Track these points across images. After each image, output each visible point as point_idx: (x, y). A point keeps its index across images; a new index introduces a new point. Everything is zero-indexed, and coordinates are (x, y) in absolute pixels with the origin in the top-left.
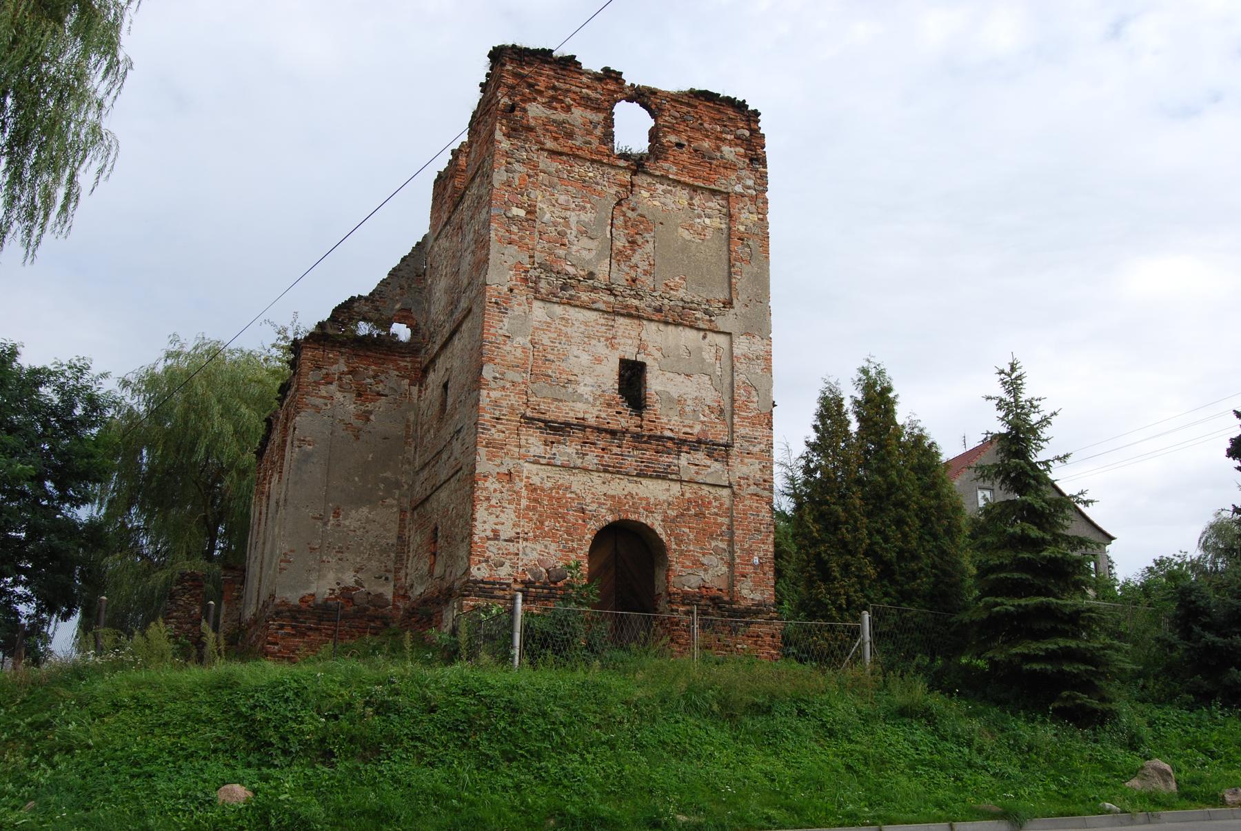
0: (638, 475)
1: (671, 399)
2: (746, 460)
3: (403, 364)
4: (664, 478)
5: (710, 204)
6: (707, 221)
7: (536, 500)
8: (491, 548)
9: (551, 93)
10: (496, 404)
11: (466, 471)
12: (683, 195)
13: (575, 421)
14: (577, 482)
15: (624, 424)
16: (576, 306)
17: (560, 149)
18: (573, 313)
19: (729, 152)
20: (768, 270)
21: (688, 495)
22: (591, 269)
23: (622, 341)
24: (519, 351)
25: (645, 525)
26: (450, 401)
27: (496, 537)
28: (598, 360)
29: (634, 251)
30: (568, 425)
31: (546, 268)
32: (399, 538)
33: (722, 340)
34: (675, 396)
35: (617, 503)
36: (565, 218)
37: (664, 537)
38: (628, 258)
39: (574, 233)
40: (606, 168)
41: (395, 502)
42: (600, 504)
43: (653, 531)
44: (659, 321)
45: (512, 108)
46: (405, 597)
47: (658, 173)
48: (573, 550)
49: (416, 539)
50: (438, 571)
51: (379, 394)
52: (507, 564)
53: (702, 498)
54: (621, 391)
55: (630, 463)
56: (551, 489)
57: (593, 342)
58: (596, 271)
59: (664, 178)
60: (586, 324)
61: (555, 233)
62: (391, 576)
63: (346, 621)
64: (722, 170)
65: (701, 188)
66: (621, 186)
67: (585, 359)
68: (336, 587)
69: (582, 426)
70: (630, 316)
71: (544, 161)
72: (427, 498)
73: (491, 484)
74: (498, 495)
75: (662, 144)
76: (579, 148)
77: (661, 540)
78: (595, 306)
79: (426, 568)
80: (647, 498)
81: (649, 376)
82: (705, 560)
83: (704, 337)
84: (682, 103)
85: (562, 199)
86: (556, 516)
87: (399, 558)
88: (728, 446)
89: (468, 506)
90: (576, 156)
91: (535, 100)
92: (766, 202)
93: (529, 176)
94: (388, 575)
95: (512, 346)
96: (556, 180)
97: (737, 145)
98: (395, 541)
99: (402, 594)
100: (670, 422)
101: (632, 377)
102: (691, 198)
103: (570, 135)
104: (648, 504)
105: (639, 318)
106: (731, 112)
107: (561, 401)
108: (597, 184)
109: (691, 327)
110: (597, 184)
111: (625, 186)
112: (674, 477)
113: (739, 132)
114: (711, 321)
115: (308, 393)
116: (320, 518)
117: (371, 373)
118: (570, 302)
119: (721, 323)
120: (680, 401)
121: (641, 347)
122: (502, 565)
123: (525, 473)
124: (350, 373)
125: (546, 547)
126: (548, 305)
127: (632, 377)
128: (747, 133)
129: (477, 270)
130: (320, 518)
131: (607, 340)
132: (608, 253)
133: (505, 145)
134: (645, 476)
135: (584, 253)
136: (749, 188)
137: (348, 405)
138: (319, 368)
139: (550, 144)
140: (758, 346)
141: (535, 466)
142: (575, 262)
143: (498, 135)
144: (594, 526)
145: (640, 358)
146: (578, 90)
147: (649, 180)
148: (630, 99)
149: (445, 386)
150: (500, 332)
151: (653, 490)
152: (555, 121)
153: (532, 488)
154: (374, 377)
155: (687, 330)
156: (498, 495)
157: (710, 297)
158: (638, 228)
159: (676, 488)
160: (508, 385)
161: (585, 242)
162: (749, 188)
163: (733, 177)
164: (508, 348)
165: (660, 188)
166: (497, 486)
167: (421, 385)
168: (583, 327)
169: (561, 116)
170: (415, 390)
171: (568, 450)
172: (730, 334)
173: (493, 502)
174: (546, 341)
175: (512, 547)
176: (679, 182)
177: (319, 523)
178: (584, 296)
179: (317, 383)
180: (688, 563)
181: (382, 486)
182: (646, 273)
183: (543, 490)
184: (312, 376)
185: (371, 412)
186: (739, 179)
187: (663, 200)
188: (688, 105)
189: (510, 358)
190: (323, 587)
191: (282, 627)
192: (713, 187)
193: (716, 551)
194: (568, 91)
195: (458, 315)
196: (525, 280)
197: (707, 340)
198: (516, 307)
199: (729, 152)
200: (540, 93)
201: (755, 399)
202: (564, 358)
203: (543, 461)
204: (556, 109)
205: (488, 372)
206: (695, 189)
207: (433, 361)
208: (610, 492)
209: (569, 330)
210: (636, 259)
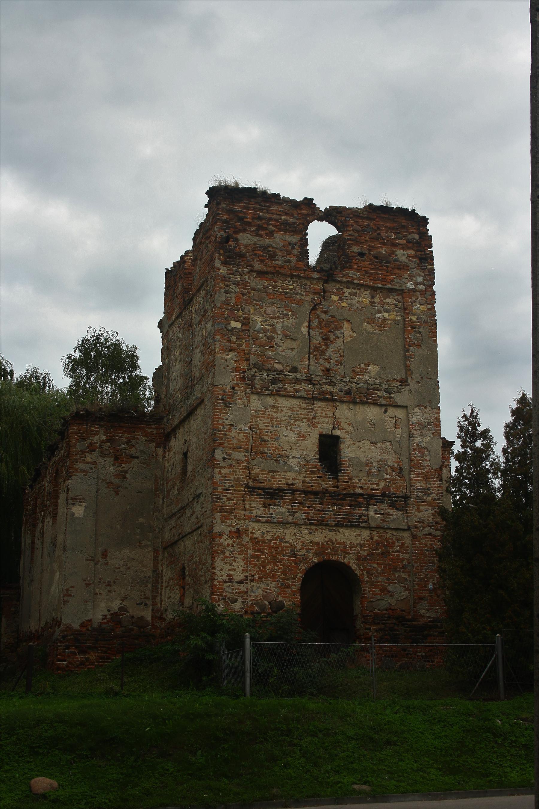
0: (336, 525)
1: (360, 464)
2: (421, 508)
3: (149, 431)
4: (357, 526)
5: (388, 300)
6: (386, 315)
7: (259, 550)
8: (227, 589)
9: (257, 222)
10: (225, 478)
11: (205, 529)
12: (366, 294)
13: (286, 487)
14: (290, 535)
15: (324, 486)
16: (284, 396)
17: (266, 269)
18: (284, 403)
19: (401, 255)
20: (436, 351)
21: (376, 538)
22: (294, 365)
23: (321, 420)
24: (241, 435)
25: (344, 564)
26: (190, 468)
27: (230, 579)
28: (302, 437)
29: (327, 346)
30: (281, 490)
31: (259, 367)
32: (154, 571)
33: (400, 413)
34: (364, 460)
35: (320, 548)
36: (272, 325)
37: (358, 572)
38: (323, 352)
39: (280, 337)
40: (304, 281)
41: (149, 543)
42: (308, 550)
43: (350, 568)
44: (349, 402)
45: (227, 239)
46: (161, 618)
47: (344, 280)
48: (289, 586)
49: (167, 574)
50: (187, 601)
51: (132, 457)
52: (240, 600)
53: (387, 540)
54: (321, 460)
55: (330, 516)
56: (270, 541)
57: (298, 423)
58: (299, 366)
59: (349, 284)
60: (291, 409)
61: (265, 338)
62: (149, 602)
63: (124, 645)
64: (397, 271)
65: (380, 288)
66: (315, 293)
67: (292, 437)
68: (106, 613)
69: (292, 490)
70: (325, 400)
71: (255, 282)
72: (175, 543)
73: (226, 541)
74: (231, 548)
75: (347, 256)
76: (281, 267)
77: (356, 574)
78: (298, 394)
79: (178, 597)
80: (344, 543)
81: (342, 446)
82: (390, 588)
83: (386, 411)
84: (363, 218)
85: (270, 310)
86: (274, 561)
87: (155, 588)
88: (406, 497)
89: (209, 557)
90: (278, 273)
91: (245, 230)
92: (433, 294)
93: (243, 295)
94: (147, 601)
95: (236, 432)
96: (264, 295)
97: (409, 248)
98: (150, 574)
99: (158, 616)
100: (361, 482)
101: (329, 447)
102: (373, 297)
103: (273, 256)
104: (345, 547)
105: (334, 401)
106: (404, 222)
107: (275, 472)
108: (297, 294)
109: (375, 404)
110: (297, 294)
111: (319, 294)
112: (364, 525)
113: (410, 237)
114: (391, 398)
115: (76, 461)
116: (92, 559)
117: (125, 440)
118: (279, 394)
119: (399, 398)
120: (368, 464)
121: (336, 424)
122: (235, 601)
123: (250, 530)
124: (107, 441)
125: (268, 585)
126: (263, 397)
127: (329, 447)
128: (417, 237)
129: (207, 370)
130: (92, 559)
131: (308, 420)
132: (307, 350)
133: (223, 271)
134: (342, 526)
135: (288, 352)
136: (419, 283)
137: (108, 468)
138: (85, 439)
139: (258, 266)
140: (428, 415)
141: (257, 524)
142: (281, 360)
143: (217, 264)
144: (304, 567)
145: (337, 432)
146: (278, 217)
147: (338, 286)
148: (320, 219)
149: (185, 455)
150: (227, 422)
151: (347, 536)
152: (261, 247)
153: (255, 541)
154: (127, 443)
155: (372, 406)
156: (231, 548)
157: (390, 378)
158: (330, 327)
159: (366, 534)
160: (234, 463)
161: (289, 343)
162: (419, 283)
163: (406, 276)
164: (233, 434)
165: (347, 291)
166: (230, 541)
167: (165, 448)
168: (290, 412)
169: (267, 241)
170: (160, 451)
171: (281, 511)
172: (406, 407)
173: (227, 554)
174: (262, 426)
175: (242, 588)
176: (362, 285)
177: (92, 563)
178: (290, 388)
179: (84, 452)
180: (377, 591)
181: (138, 531)
182: (338, 363)
183: (264, 542)
184: (79, 447)
185: (126, 472)
186: (411, 277)
187: (350, 301)
188: (368, 219)
189: (235, 441)
190: (98, 613)
191: (68, 647)
192: (389, 286)
193: (401, 580)
194: (270, 219)
195: (192, 401)
196: (243, 379)
197: (388, 414)
198: (238, 402)
199: (401, 255)
200: (249, 224)
201: (428, 458)
202: (276, 437)
203: (263, 520)
204: (261, 236)
205: (219, 454)
206: (375, 289)
207: (174, 430)
208: (316, 540)
209: (279, 415)
210: (330, 351)
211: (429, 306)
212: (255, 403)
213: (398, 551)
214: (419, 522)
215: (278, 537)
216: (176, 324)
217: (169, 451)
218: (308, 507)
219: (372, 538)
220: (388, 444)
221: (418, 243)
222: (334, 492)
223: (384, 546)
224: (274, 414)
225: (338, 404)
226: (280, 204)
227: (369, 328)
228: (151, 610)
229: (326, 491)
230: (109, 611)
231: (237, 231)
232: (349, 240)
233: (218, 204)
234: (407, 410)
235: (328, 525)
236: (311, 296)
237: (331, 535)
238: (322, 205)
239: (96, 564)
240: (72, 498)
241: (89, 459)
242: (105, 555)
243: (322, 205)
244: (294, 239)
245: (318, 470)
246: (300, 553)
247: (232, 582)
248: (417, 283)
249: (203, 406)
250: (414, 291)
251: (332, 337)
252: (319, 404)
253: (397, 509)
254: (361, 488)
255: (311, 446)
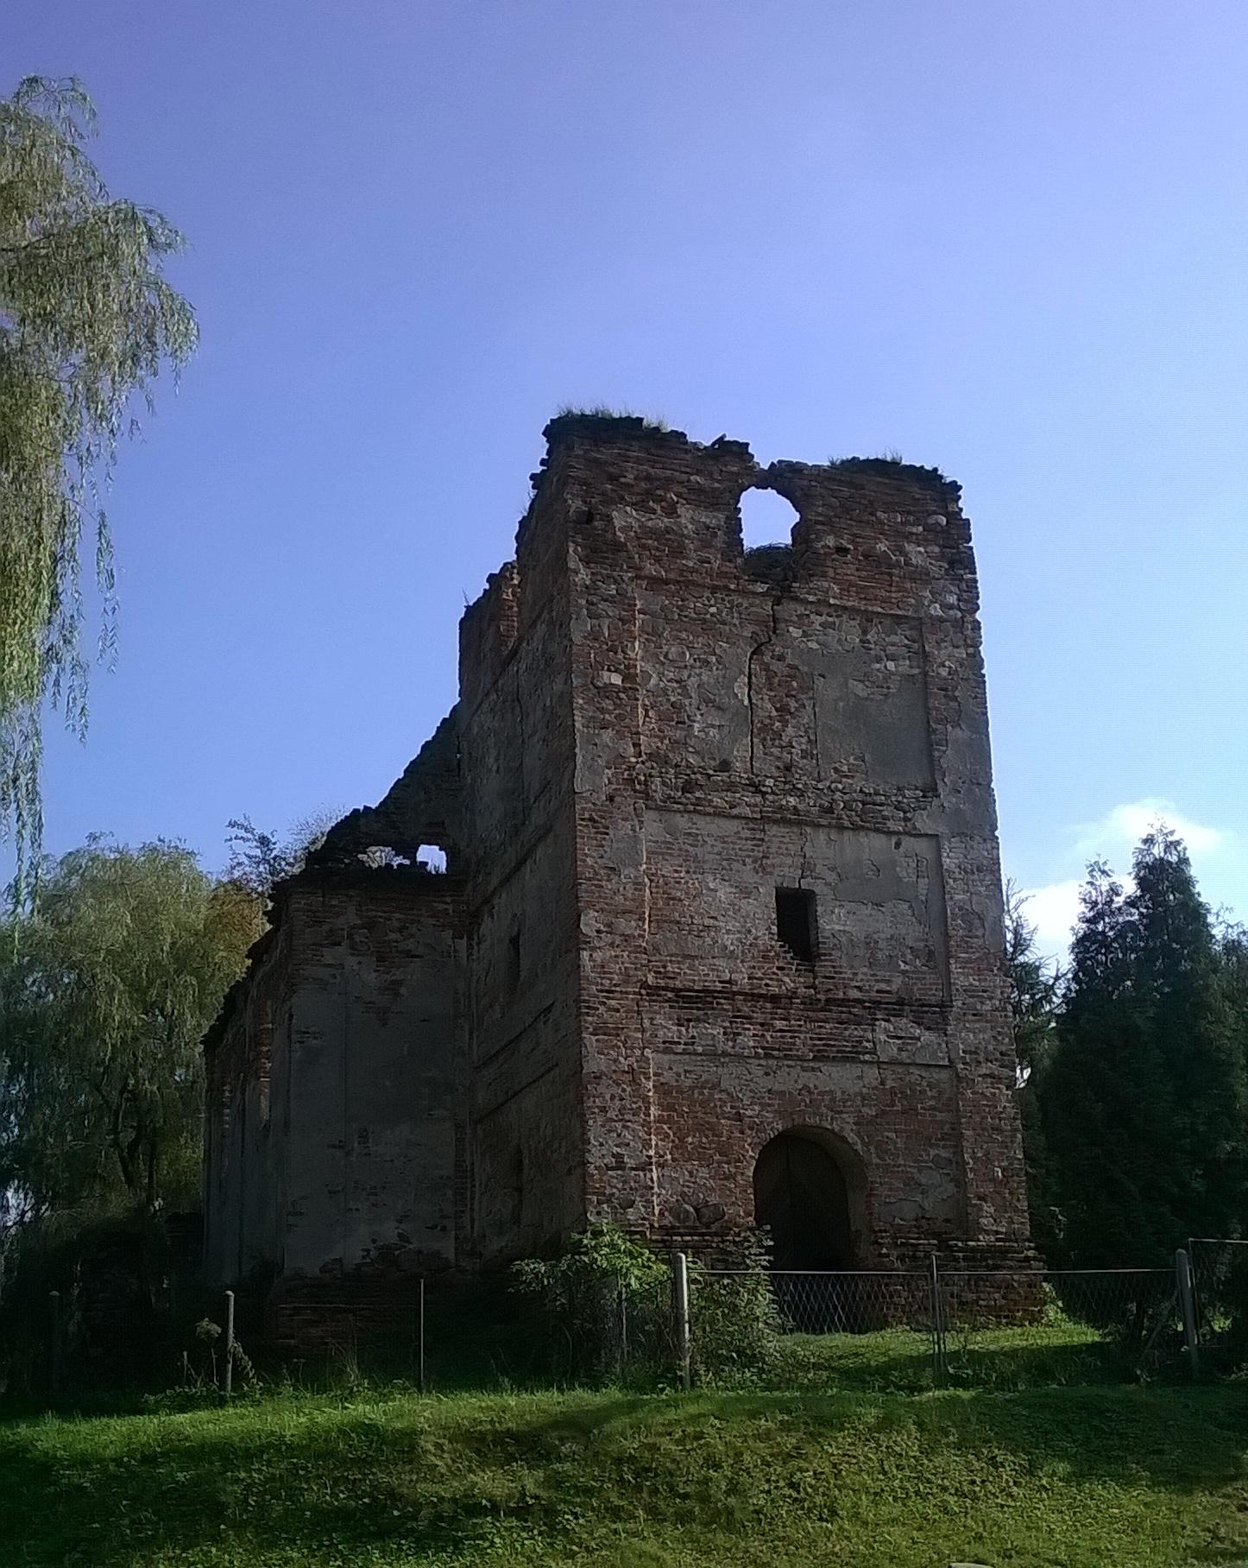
4: (853, 1060)
6: (891, 665)
13: (719, 986)
14: (728, 1077)
19: (917, 554)
21: (889, 1084)
23: (777, 861)
26: (525, 963)
29: (785, 724)
33: (922, 847)
43: (844, 1139)
44: (829, 826)
45: (589, 517)
51: (410, 955)
56: (692, 1089)
57: (735, 866)
68: (371, 1246)
69: (729, 991)
70: (784, 821)
78: (734, 812)
83: (898, 845)
86: (700, 1128)
92: (977, 626)
100: (858, 978)
101: (795, 914)
102: (865, 632)
104: (833, 1100)
105: (800, 823)
106: (916, 491)
112: (867, 1057)
117: (396, 924)
118: (697, 809)
119: (924, 822)
120: (870, 943)
121: (806, 868)
126: (667, 816)
127: (795, 914)
136: (951, 607)
138: (318, 923)
139: (650, 568)
141: (667, 1057)
147: (801, 610)
149: (515, 942)
151: (839, 1078)
155: (872, 834)
158: (790, 688)
159: (872, 1074)
165: (818, 620)
176: (845, 608)
190: (352, 1249)
194: (669, 480)
197: (902, 849)
199: (917, 554)
201: (980, 933)
206: (869, 617)
208: (776, 1087)
211: (971, 650)
212: (652, 828)
213: (933, 1108)
214: (971, 1053)
215: (706, 1081)
216: (485, 707)
217: (479, 944)
218: (762, 1025)
219: (882, 1083)
220: (906, 906)
221: (945, 531)
222: (810, 997)
223: (906, 1097)
224: (691, 849)
225: (809, 830)
226: (687, 452)
227: (860, 690)
228: (453, 1240)
229: (793, 994)
230: (374, 1241)
231: (608, 501)
232: (817, 522)
233: (570, 448)
234: (938, 843)
235: (799, 1058)
236: (751, 628)
237: (809, 1079)
238: (764, 459)
239: (348, 1154)
240: (299, 1032)
241: (328, 960)
242: (364, 1138)
243: (764, 459)
244: (716, 519)
245: (777, 955)
246: (749, 1113)
247: (623, 1169)
248: (947, 607)
249: (551, 835)
250: (941, 620)
251: (793, 704)
252: (774, 830)
253: (928, 1029)
254: (859, 988)
255: (761, 913)
